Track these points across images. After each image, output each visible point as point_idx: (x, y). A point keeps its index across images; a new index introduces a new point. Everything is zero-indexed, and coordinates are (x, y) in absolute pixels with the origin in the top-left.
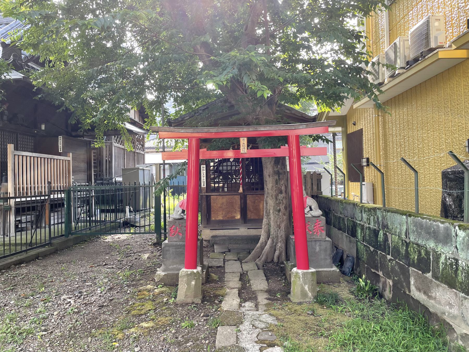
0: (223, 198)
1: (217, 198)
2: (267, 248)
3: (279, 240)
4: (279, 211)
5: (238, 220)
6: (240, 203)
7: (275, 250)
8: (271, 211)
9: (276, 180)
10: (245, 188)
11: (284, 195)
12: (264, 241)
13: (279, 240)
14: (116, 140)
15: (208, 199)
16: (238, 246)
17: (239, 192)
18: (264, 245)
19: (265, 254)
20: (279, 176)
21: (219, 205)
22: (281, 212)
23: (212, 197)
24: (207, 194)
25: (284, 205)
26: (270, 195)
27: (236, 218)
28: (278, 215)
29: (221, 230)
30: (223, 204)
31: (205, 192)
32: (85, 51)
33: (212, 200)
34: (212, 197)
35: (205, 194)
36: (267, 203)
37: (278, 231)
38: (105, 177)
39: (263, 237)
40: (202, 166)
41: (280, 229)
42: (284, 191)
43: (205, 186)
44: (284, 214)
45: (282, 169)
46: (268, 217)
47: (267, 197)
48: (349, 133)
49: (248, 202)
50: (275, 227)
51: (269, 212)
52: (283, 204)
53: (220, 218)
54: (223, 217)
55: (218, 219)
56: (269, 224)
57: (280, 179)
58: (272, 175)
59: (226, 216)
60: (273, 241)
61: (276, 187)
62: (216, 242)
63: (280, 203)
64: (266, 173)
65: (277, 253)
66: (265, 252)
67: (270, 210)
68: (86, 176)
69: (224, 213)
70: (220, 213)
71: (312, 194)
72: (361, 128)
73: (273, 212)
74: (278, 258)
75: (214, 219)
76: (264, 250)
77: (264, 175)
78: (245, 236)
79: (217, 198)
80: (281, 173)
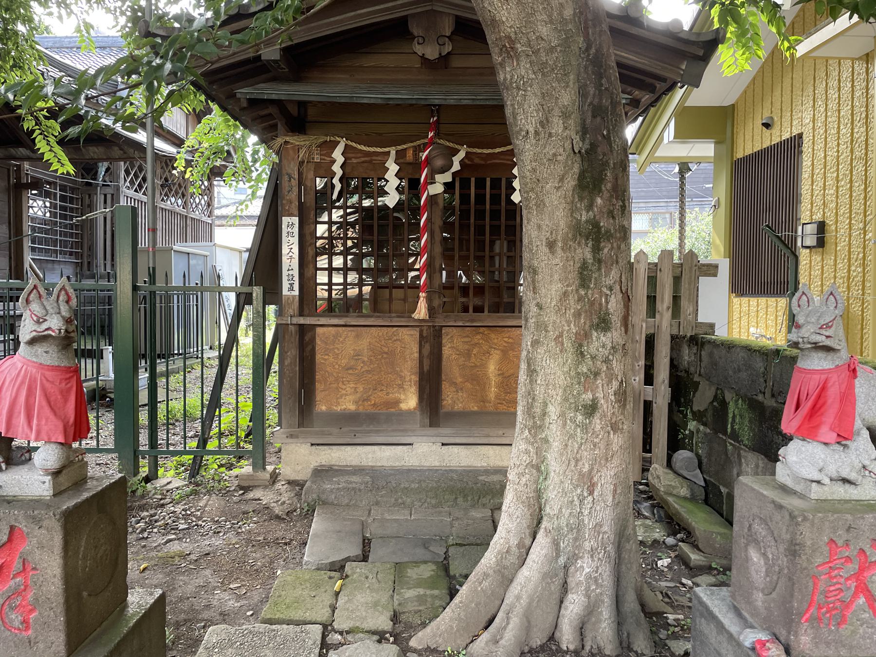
0: (358, 336)
1: (336, 336)
2: (528, 580)
3: (587, 545)
4: (591, 409)
5: (409, 412)
6: (416, 355)
7: (565, 589)
8: (553, 410)
9: (584, 266)
10: (436, 303)
11: (615, 335)
12: (514, 541)
13: (587, 545)
14: (132, 182)
15: (307, 338)
16: (402, 515)
17: (416, 316)
18: (512, 559)
19: (519, 610)
20: (596, 249)
21: (344, 362)
22: (597, 415)
23: (319, 330)
24: (302, 321)
25: (615, 384)
26: (552, 334)
27: (403, 406)
28: (585, 428)
29: (349, 448)
30: (357, 355)
31: (297, 312)
32: (168, 66)
33: (318, 341)
34: (319, 330)
35: (296, 320)
36: (532, 372)
37: (581, 502)
38: (101, 270)
39: (512, 526)
40: (286, 220)
41: (591, 493)
42: (616, 320)
43: (296, 292)
44: (615, 427)
45: (611, 214)
46: (535, 437)
47: (536, 343)
48: (740, 155)
49: (446, 351)
50: (567, 485)
51: (544, 414)
52: (610, 379)
53: (348, 405)
54: (356, 402)
55: (339, 409)
56: (538, 469)
57: (600, 261)
58: (565, 243)
59: (367, 399)
60: (556, 544)
61: (580, 299)
62: (324, 497)
63: (596, 374)
64: (534, 233)
65: (574, 605)
66: (518, 598)
67: (545, 405)
68: (7, 260)
69: (361, 389)
70: (349, 387)
71: (675, 332)
72: (795, 132)
73: (562, 415)
74: (581, 630)
75: (324, 408)
76: (515, 589)
77: (525, 241)
78: (433, 471)
79: (336, 336)
80: (609, 236)
